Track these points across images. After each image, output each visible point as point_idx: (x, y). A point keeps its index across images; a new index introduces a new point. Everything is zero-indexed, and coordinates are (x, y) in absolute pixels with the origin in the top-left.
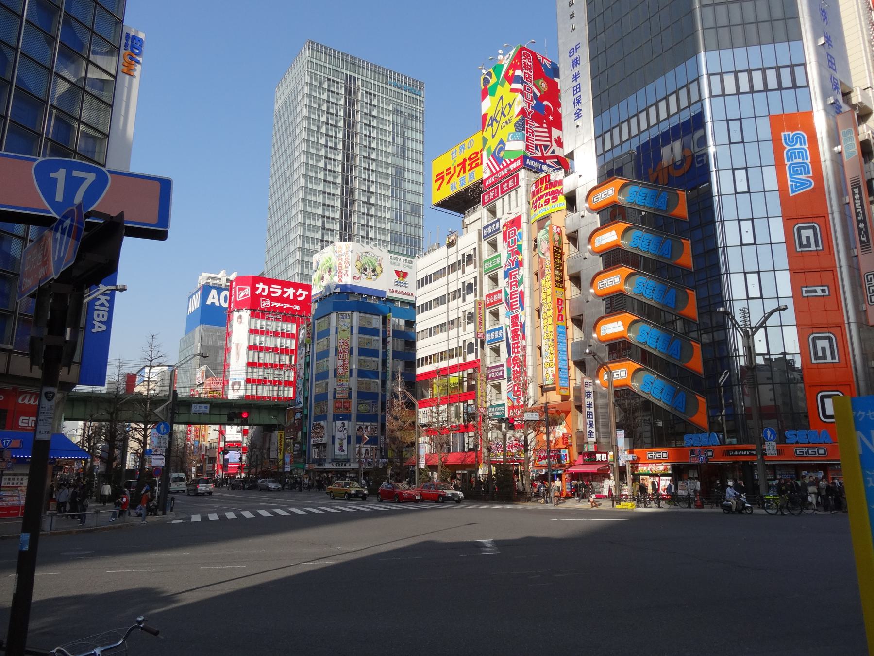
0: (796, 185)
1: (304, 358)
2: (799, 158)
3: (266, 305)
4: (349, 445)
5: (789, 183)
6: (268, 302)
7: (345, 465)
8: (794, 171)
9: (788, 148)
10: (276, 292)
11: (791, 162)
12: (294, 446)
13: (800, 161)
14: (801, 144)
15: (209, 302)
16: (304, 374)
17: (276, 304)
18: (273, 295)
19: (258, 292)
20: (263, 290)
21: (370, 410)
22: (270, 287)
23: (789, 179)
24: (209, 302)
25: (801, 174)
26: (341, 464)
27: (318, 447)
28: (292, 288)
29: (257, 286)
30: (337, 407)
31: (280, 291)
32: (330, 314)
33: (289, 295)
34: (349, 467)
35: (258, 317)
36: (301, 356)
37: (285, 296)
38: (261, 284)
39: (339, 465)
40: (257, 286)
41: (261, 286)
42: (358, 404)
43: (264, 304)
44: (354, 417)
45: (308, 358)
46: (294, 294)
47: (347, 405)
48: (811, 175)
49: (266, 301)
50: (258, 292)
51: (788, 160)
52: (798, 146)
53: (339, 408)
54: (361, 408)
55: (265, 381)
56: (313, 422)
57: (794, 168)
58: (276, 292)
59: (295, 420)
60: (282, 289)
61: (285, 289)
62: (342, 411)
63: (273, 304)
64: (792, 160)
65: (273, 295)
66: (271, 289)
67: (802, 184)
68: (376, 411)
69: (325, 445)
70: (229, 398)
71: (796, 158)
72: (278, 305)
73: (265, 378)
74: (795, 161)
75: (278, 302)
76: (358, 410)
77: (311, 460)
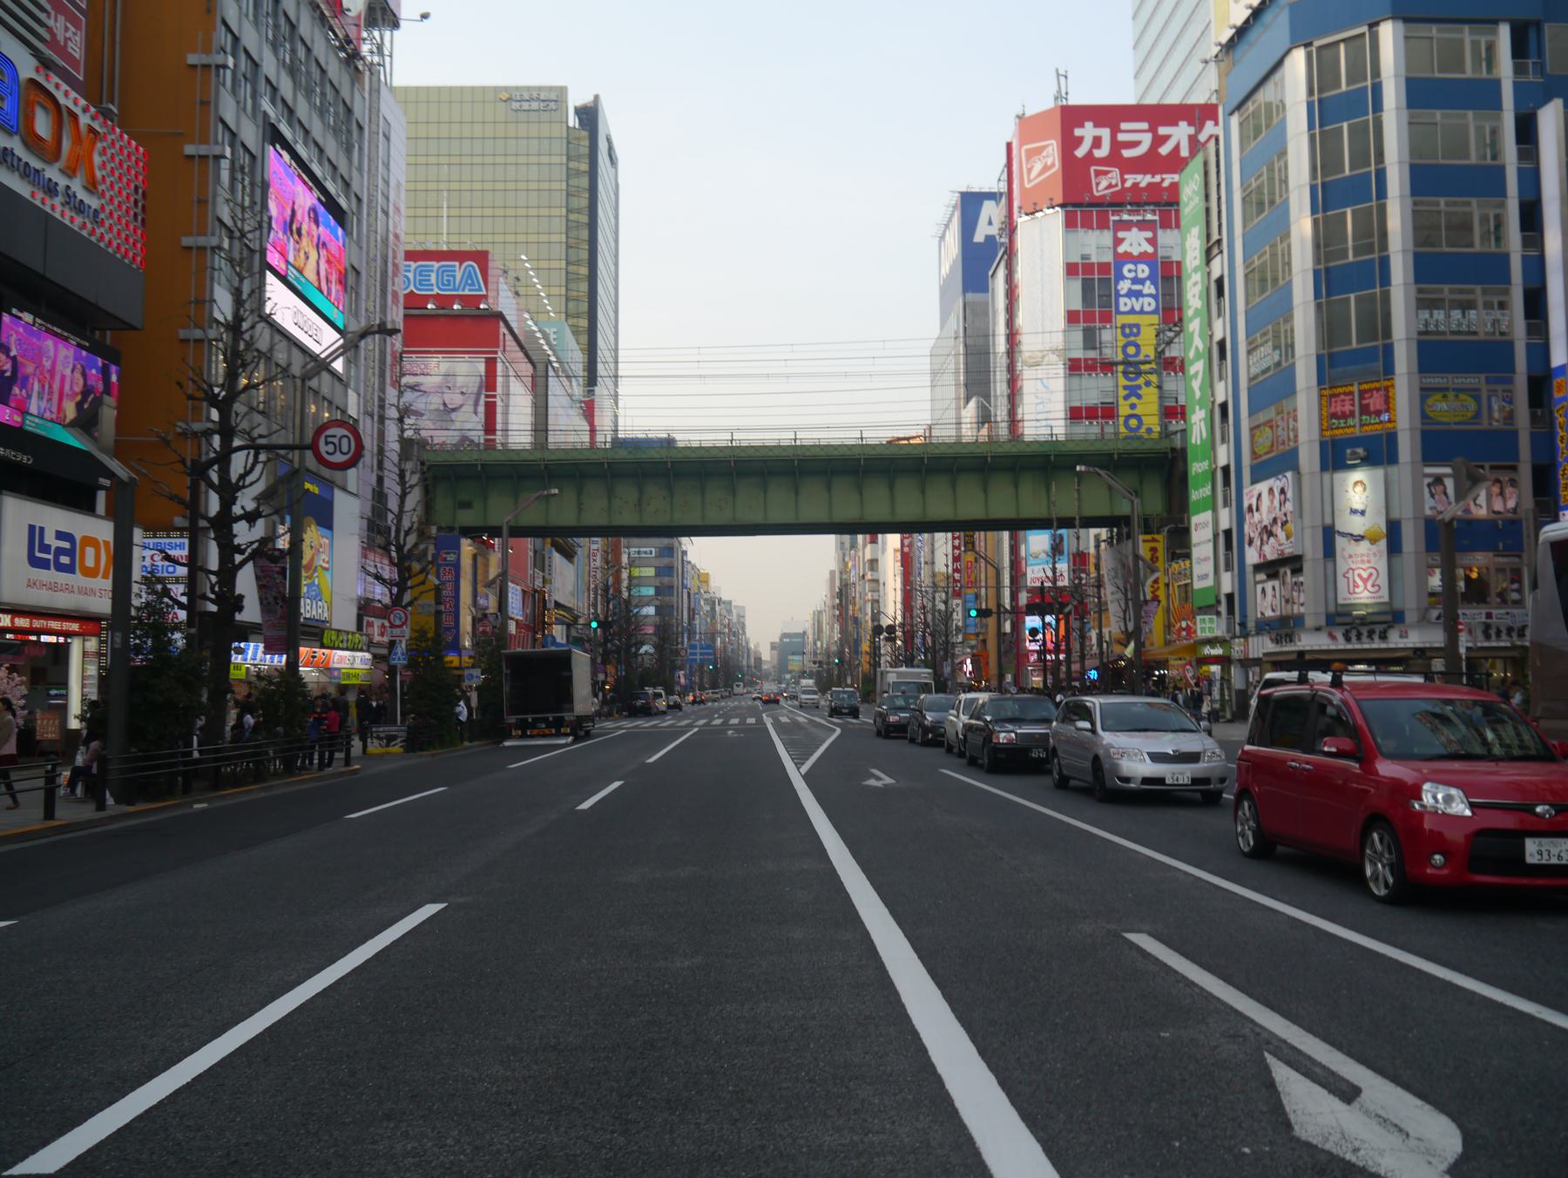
0: (470, 285)
2: (429, 276)
3: (1110, 186)
4: (1396, 560)
5: (467, 292)
6: (1115, 174)
7: (1383, 637)
8: (449, 285)
10: (1135, 144)
13: (433, 276)
14: (409, 271)
15: (979, 237)
17: (1139, 177)
18: (1127, 153)
19: (1080, 152)
20: (1097, 142)
21: (1478, 415)
22: (1115, 131)
23: (460, 293)
24: (979, 237)
25: (454, 277)
26: (1364, 631)
27: (1272, 576)
28: (1183, 124)
29: (1078, 132)
30: (1334, 416)
31: (1147, 139)
32: (1279, 64)
33: (1177, 148)
34: (1401, 643)
35: (1087, 225)
37: (1164, 150)
38: (1089, 125)
39: (1359, 636)
40: (1078, 132)
41: (1088, 131)
42: (1426, 392)
43: (1104, 184)
44: (1406, 446)
46: (1193, 140)
47: (1375, 401)
48: (457, 264)
49: (1106, 173)
50: (1080, 152)
51: (432, 290)
52: (410, 275)
53: (1344, 416)
54: (1441, 407)
57: (443, 284)
58: (1135, 144)
60: (1153, 129)
61: (1162, 131)
62: (1354, 427)
63: (1131, 179)
64: (432, 285)
65: (1127, 153)
66: (1121, 137)
67: (470, 276)
68: (1510, 417)
69: (1294, 563)
70: (1027, 439)
71: (429, 280)
72: (1144, 180)
74: (433, 281)
75: (1144, 172)
76: (1424, 416)
77: (1251, 625)
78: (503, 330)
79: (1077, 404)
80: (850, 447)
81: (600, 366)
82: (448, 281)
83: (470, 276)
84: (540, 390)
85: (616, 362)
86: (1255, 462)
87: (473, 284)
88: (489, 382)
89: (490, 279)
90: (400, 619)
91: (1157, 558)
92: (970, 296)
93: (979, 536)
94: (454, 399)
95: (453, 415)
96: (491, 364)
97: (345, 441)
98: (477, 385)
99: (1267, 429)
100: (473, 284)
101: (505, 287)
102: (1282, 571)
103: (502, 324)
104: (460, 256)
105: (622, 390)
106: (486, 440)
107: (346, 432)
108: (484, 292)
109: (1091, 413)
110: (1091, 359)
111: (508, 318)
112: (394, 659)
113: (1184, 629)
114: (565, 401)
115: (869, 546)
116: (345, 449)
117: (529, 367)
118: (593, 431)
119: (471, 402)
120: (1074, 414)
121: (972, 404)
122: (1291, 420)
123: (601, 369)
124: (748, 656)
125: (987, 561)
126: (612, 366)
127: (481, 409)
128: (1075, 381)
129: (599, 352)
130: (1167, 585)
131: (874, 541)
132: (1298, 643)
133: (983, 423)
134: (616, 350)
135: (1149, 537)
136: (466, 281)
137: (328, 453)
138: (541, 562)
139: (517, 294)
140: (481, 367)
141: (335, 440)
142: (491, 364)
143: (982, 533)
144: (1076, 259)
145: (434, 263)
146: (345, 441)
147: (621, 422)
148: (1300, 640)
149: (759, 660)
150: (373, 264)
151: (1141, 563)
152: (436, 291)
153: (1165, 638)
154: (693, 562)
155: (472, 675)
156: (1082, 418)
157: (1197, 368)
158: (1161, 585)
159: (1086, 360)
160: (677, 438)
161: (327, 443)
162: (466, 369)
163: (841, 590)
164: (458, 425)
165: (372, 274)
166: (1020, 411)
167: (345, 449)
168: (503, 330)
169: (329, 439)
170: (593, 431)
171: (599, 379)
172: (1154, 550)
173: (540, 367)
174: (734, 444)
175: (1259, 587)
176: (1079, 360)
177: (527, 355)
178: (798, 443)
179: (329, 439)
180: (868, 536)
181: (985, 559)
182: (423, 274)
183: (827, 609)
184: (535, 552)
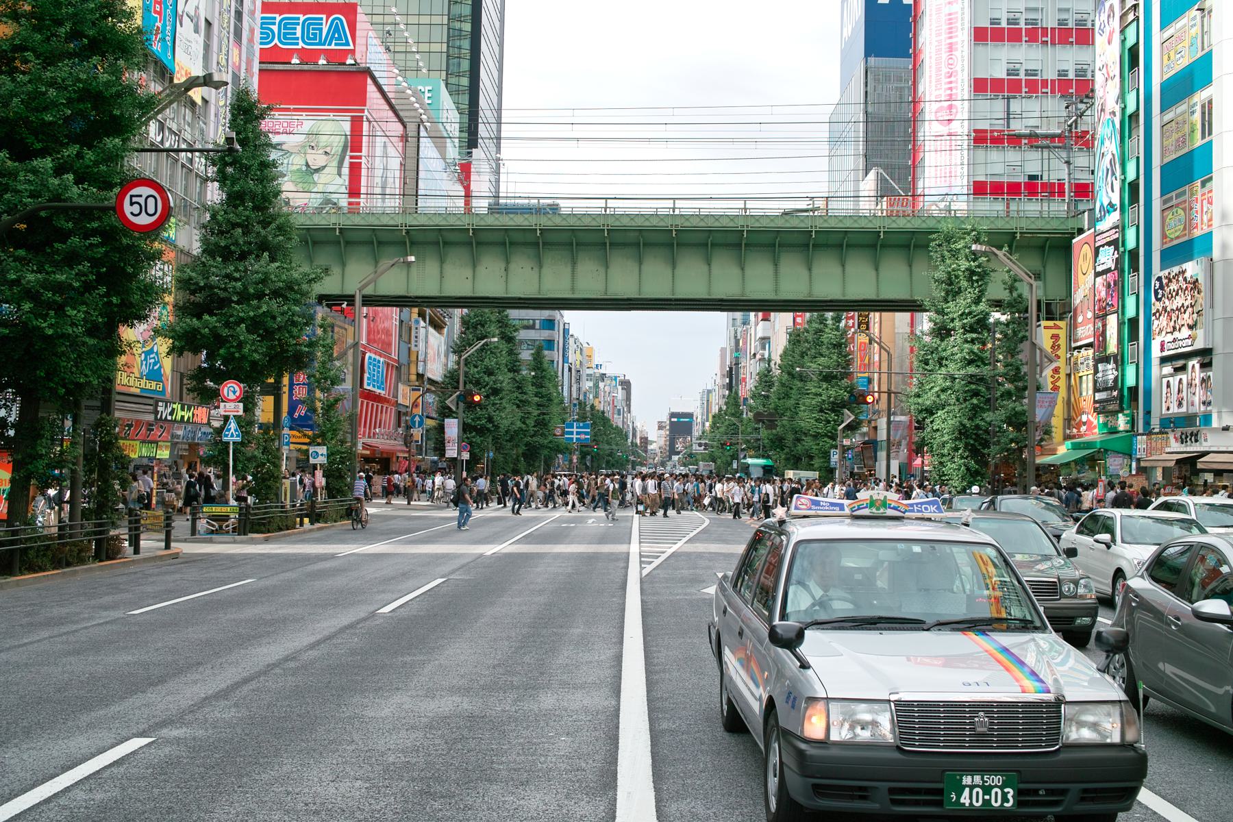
0: (337, 39)
1: (1117, 38)
2: (295, 29)
5: (333, 47)
9: (276, 41)
11: (300, 41)
12: (1096, 371)
13: (299, 28)
14: (274, 24)
16: (1122, 97)
23: (326, 47)
25: (321, 30)
36: (1107, 30)
45: (1131, 31)
48: (324, 16)
51: (298, 44)
52: (275, 28)
55: (1033, 187)
56: (1157, 271)
59: (1097, 274)
64: (298, 39)
67: (337, 30)
71: (295, 34)
73: (1031, 177)
74: (299, 34)
77: (1155, 423)
78: (371, 88)
79: (982, 179)
80: (732, 218)
81: (481, 127)
82: (315, 34)
83: (337, 30)
84: (411, 151)
85: (499, 123)
86: (1166, 246)
87: (340, 38)
88: (355, 142)
89: (358, 33)
90: (234, 392)
91: (1059, 346)
92: (872, 60)
93: (875, 317)
94: (317, 160)
95: (316, 176)
96: (357, 123)
97: (151, 201)
98: (342, 144)
99: (1180, 211)
100: (340, 38)
101: (375, 41)
102: (1190, 364)
103: (369, 81)
104: (329, 9)
105: (505, 153)
106: (350, 204)
107: (153, 192)
108: (352, 47)
109: (997, 189)
110: (997, 131)
111: (377, 74)
112: (227, 436)
113: (1084, 424)
114: (439, 165)
115: (761, 323)
116: (151, 210)
117: (399, 127)
118: (468, 196)
119: (335, 163)
120: (979, 189)
121: (872, 175)
122: (1205, 203)
123: (482, 130)
124: (634, 435)
125: (881, 347)
126: (494, 127)
127: (346, 170)
128: (981, 153)
129: (481, 112)
130: (1069, 376)
131: (765, 319)
132: (1205, 444)
133: (882, 197)
134: (499, 110)
135: (1051, 323)
136: (334, 34)
137: (132, 213)
138: (406, 330)
139: (388, 49)
140: (347, 127)
141: (142, 201)
142: (357, 123)
143: (877, 314)
144: (985, 24)
145: (301, 16)
146: (151, 201)
147: (503, 188)
148: (1206, 440)
149: (645, 441)
150: (226, 16)
151: (1038, 351)
152: (301, 45)
153: (1064, 432)
154: (575, 336)
155: (317, 453)
156: (986, 194)
157: (1108, 146)
158: (1062, 375)
159: (992, 131)
160: (561, 205)
161: (132, 204)
162: (335, 127)
163: (731, 369)
164: (320, 188)
165: (225, 25)
166: (920, 184)
167: (151, 210)
168: (371, 88)
169: (134, 199)
170: (468, 196)
171: (480, 141)
172: (1055, 337)
173: (412, 128)
174: (608, 212)
175: (1165, 381)
176: (985, 131)
177: (397, 115)
178: (677, 212)
179: (134, 199)
180: (760, 314)
181: (879, 344)
182: (287, 26)
183: (717, 388)
184: (401, 322)
